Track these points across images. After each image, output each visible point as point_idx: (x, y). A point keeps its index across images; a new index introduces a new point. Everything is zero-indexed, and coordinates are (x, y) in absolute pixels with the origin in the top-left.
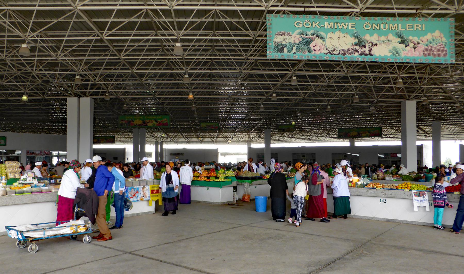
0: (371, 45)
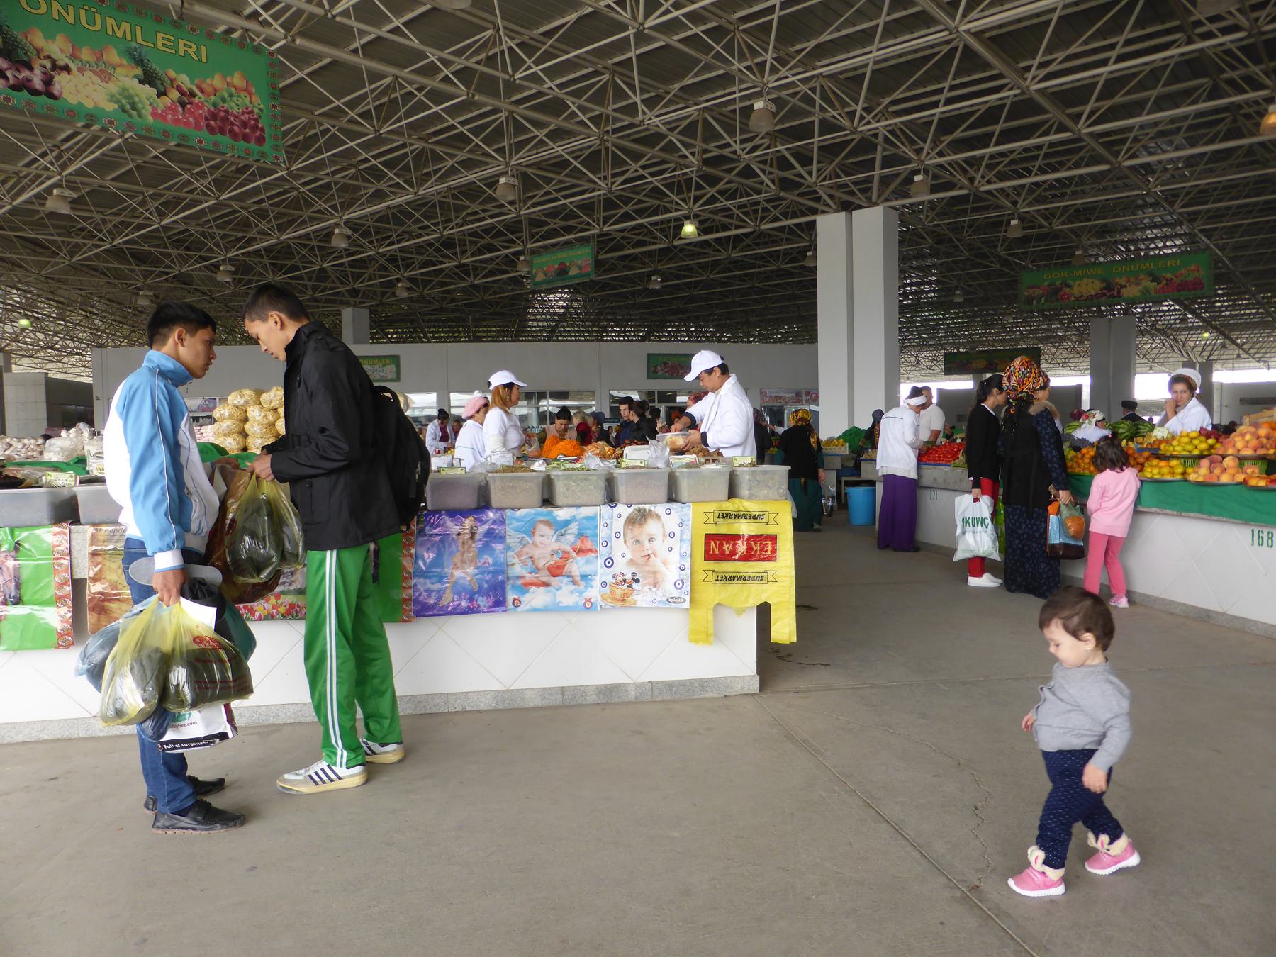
0: (48, 64)
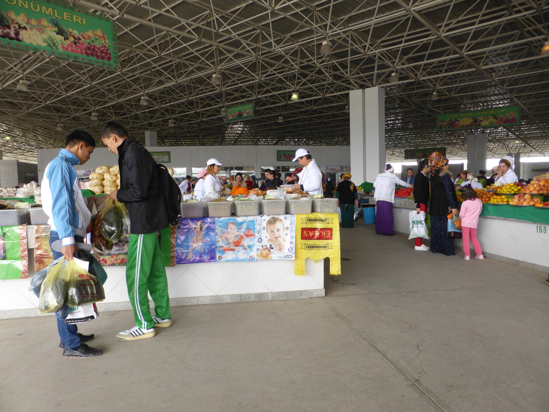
0: (17, 26)
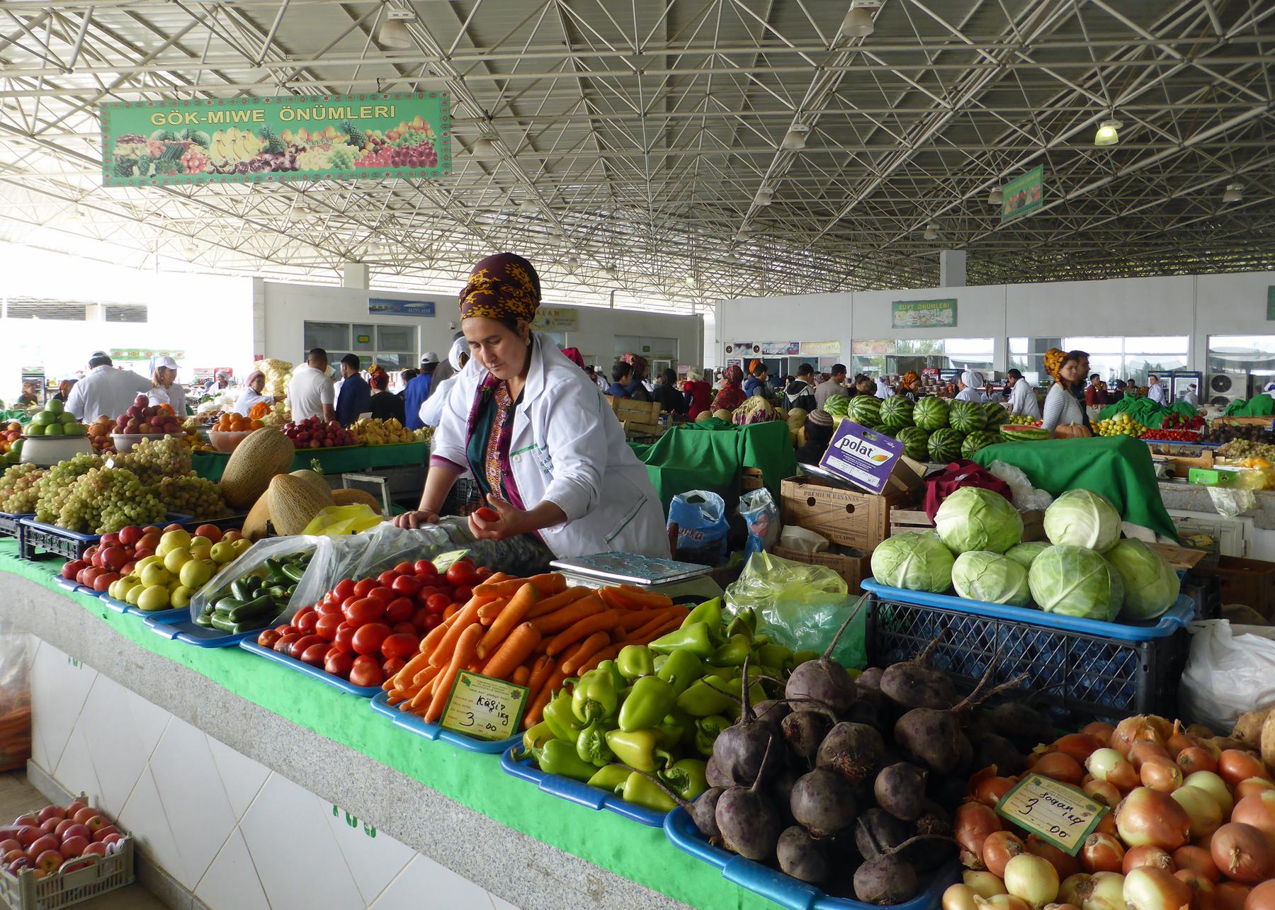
0: (293, 150)
